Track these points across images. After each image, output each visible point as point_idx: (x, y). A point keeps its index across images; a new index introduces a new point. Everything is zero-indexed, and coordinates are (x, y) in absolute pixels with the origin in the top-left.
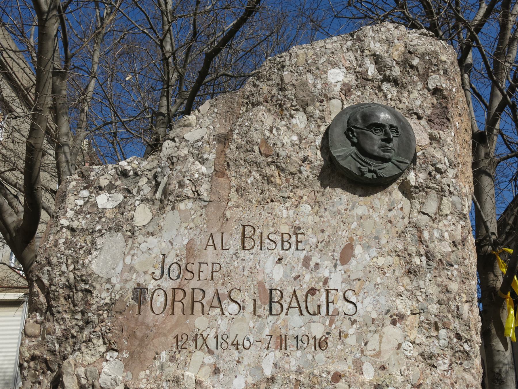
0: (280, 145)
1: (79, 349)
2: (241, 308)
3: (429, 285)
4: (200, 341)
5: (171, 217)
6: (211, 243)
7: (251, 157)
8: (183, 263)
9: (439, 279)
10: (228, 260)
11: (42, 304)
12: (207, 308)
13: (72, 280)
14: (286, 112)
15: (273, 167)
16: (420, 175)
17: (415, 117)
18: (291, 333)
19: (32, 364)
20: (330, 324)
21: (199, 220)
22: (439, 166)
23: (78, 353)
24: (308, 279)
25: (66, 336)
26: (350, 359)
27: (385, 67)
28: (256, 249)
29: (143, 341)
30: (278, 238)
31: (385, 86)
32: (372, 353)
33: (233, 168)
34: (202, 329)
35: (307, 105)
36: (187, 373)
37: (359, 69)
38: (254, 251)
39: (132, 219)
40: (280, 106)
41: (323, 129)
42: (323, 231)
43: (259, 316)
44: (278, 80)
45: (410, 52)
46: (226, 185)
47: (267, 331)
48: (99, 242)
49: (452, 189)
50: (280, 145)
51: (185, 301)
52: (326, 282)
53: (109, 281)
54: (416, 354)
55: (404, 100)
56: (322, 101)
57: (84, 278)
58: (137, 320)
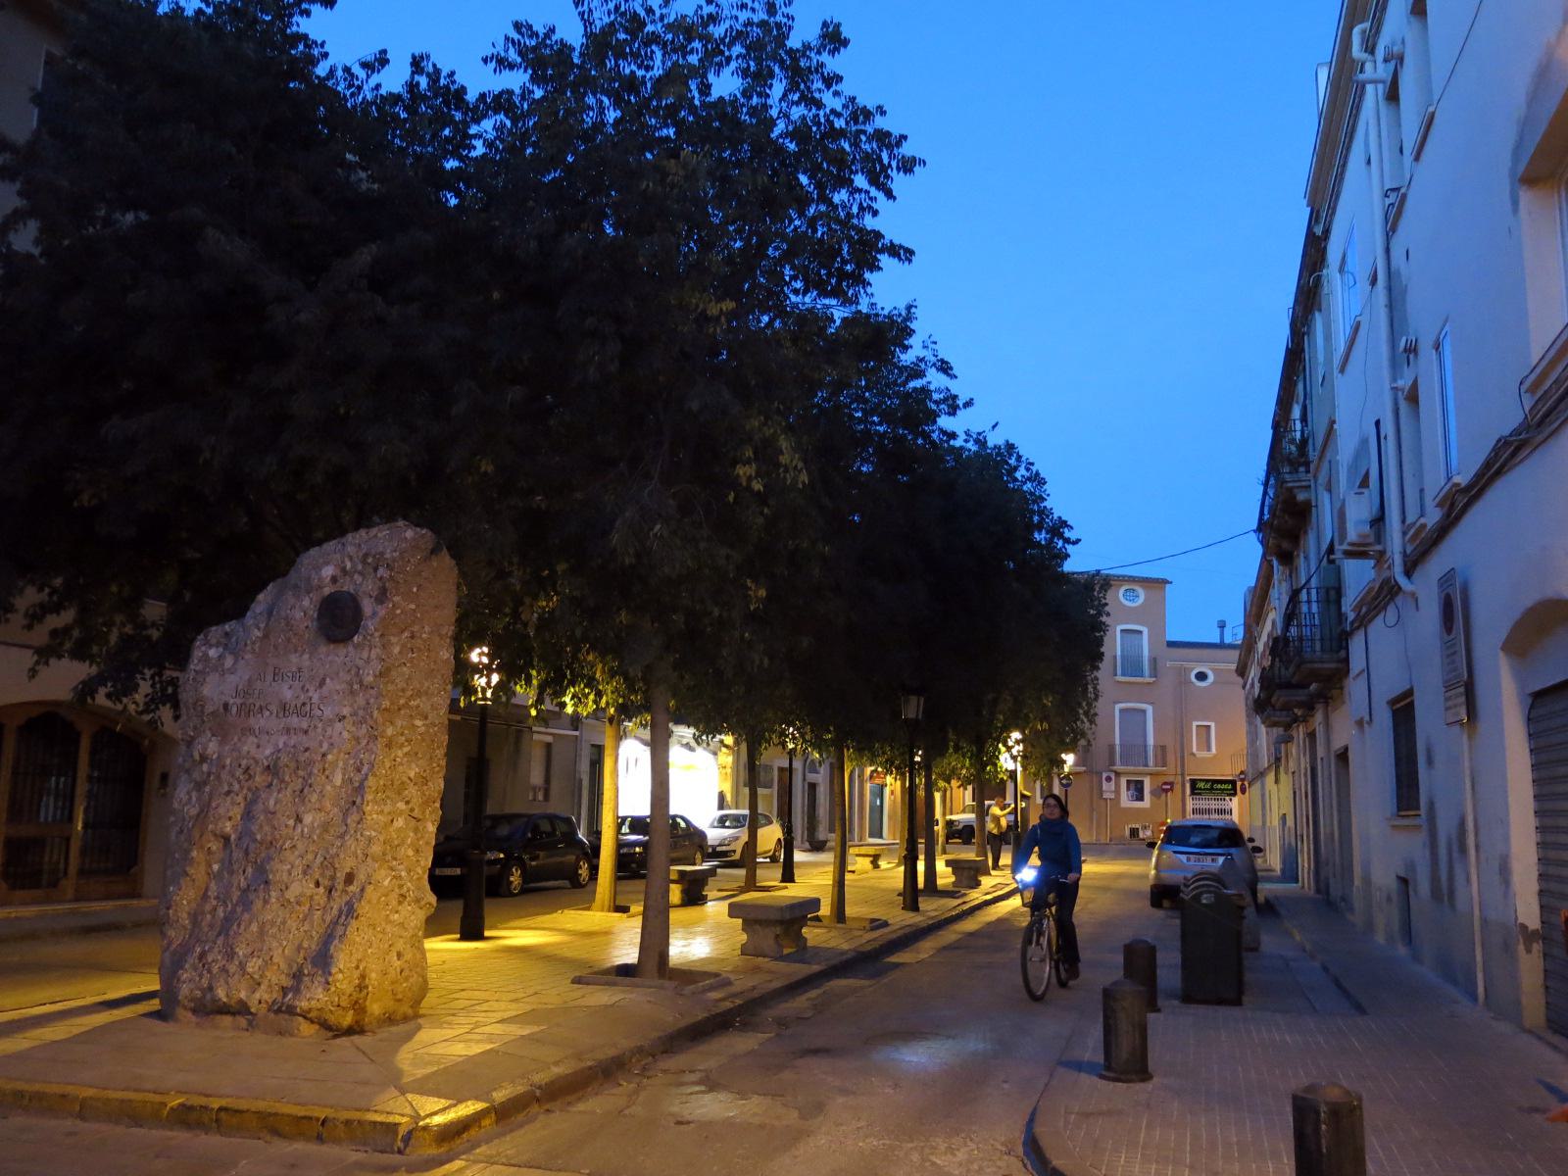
2: (271, 714)
51: (246, 710)
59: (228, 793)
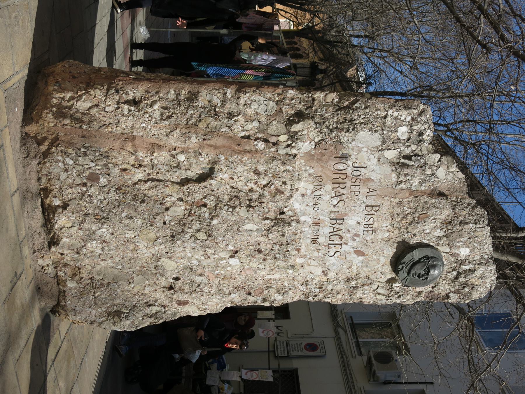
0: (424, 224)
1: (317, 128)
2: (335, 206)
3: (341, 286)
4: (318, 187)
5: (387, 169)
6: (371, 190)
7: (419, 210)
8: (361, 177)
9: (344, 290)
10: (361, 199)
11: (343, 103)
12: (335, 190)
13: (355, 122)
14: (445, 226)
15: (412, 220)
16: (398, 288)
17: (434, 286)
18: (321, 228)
19: (310, 99)
20: (324, 245)
21: (385, 184)
22: (402, 297)
23: (315, 127)
24: (347, 236)
25: (325, 119)
26: (307, 253)
27: (467, 274)
28: (366, 212)
29: (320, 160)
30: (371, 222)
31: (455, 273)
32: (309, 262)
33: (414, 199)
34: (325, 188)
35: (447, 238)
36: (302, 183)
37: (467, 261)
38: (365, 211)
39: (389, 149)
40: (450, 222)
41: (432, 244)
42: (373, 243)
43: (330, 214)
44: (468, 221)
45: (473, 287)
46: (404, 197)
47: (322, 218)
48: (377, 134)
49: (389, 301)
50: (424, 224)
51: (339, 179)
52: (345, 244)
53: (354, 140)
54: (308, 279)
55: (444, 282)
56: (448, 245)
57: (356, 129)
58: (331, 156)
59: (257, 172)
